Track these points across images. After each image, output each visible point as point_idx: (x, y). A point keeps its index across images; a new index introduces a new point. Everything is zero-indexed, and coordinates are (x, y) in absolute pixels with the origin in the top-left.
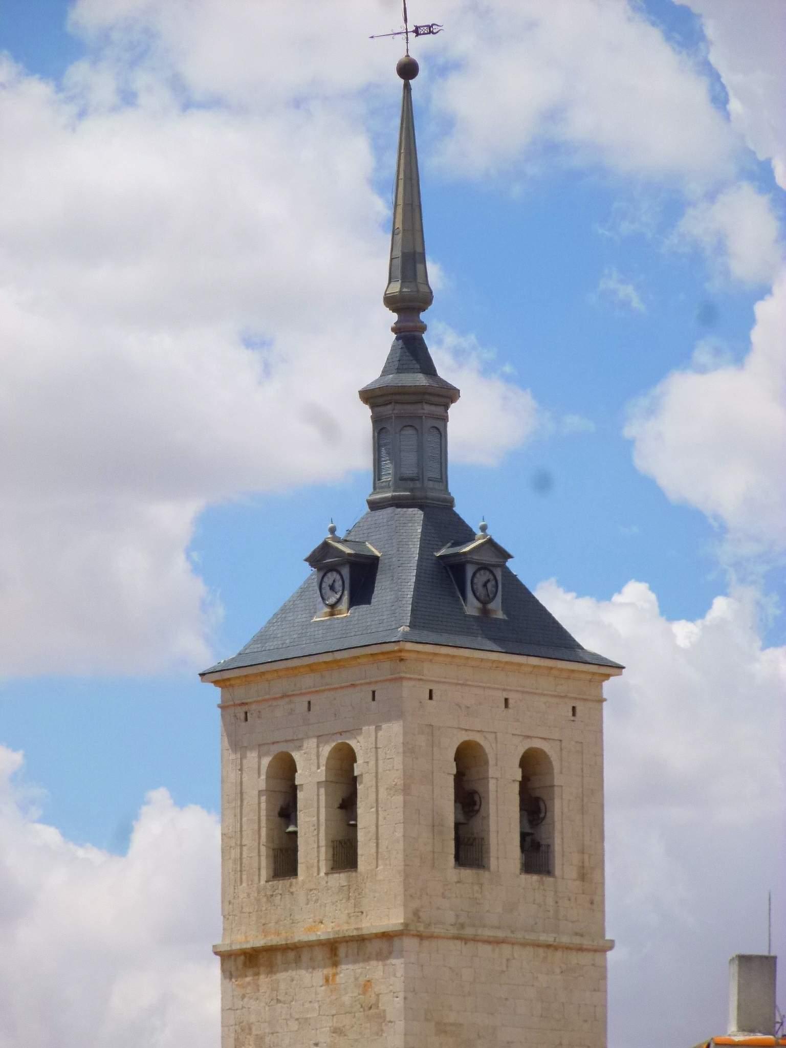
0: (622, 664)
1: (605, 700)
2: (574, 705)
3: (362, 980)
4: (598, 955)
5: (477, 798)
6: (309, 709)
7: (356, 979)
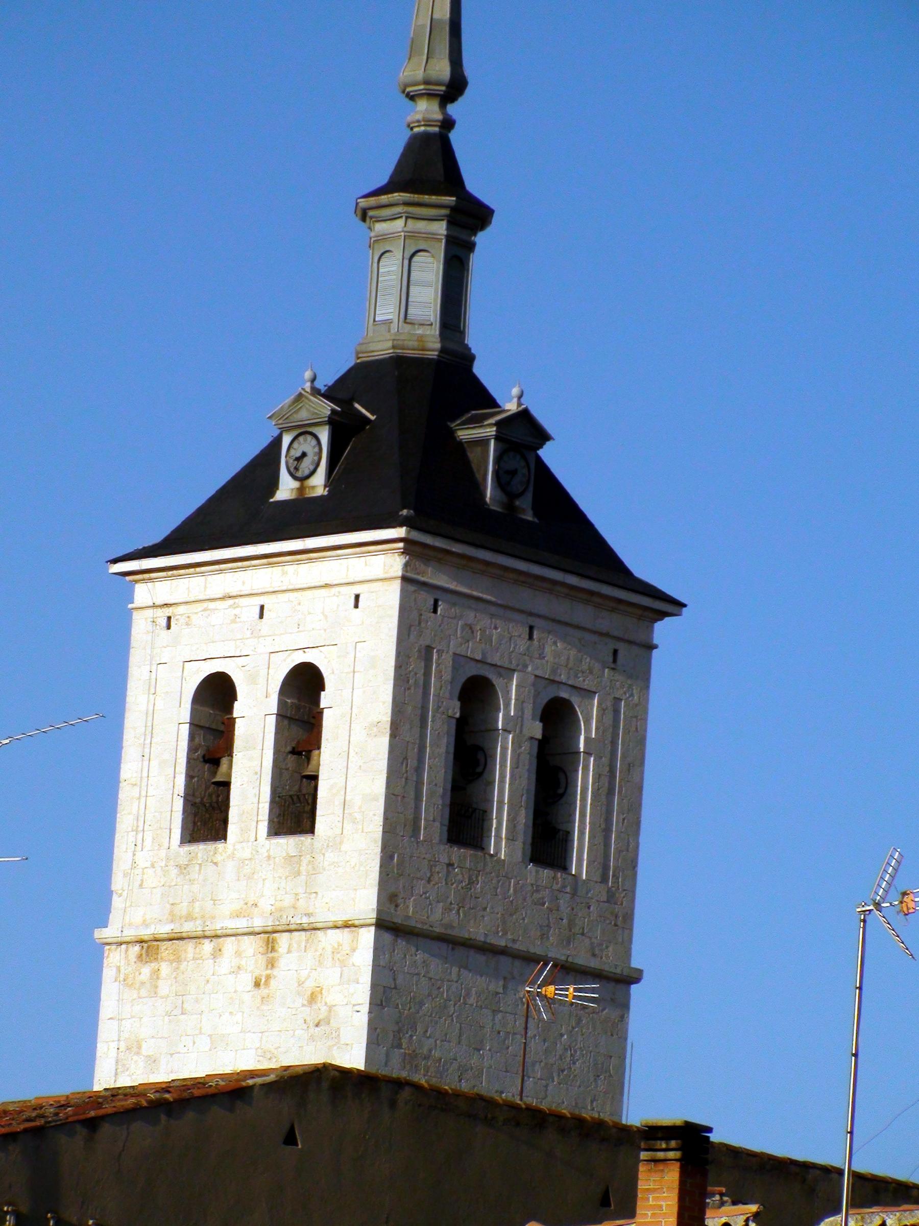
0: (683, 600)
1: (656, 647)
2: (616, 648)
3: (310, 985)
4: (621, 986)
5: (480, 756)
6: (261, 616)
7: (300, 984)
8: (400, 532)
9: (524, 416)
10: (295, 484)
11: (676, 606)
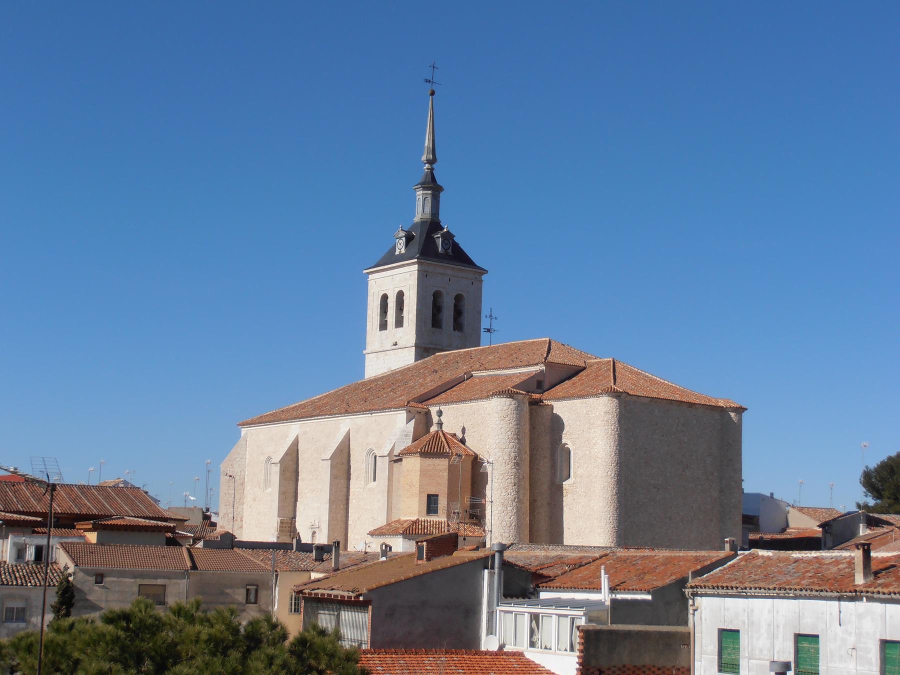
0: (746, 407)
8: (416, 260)
9: (448, 232)
10: (399, 251)
11: (486, 272)
